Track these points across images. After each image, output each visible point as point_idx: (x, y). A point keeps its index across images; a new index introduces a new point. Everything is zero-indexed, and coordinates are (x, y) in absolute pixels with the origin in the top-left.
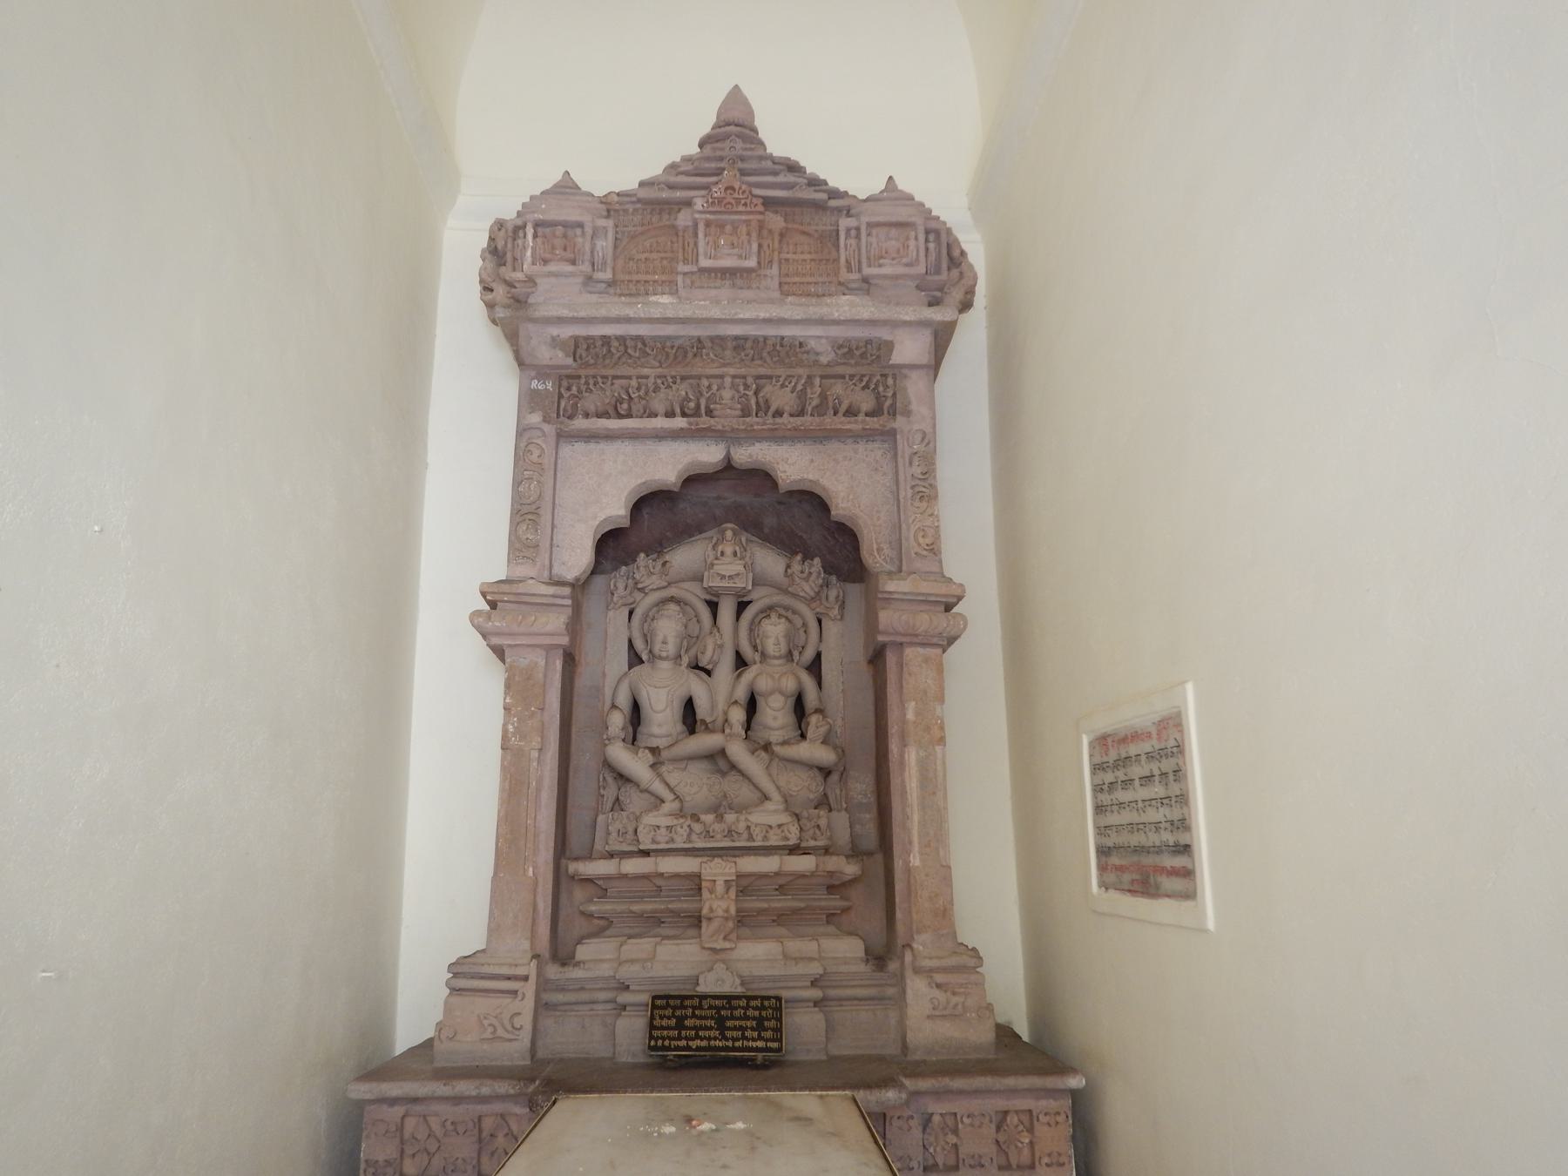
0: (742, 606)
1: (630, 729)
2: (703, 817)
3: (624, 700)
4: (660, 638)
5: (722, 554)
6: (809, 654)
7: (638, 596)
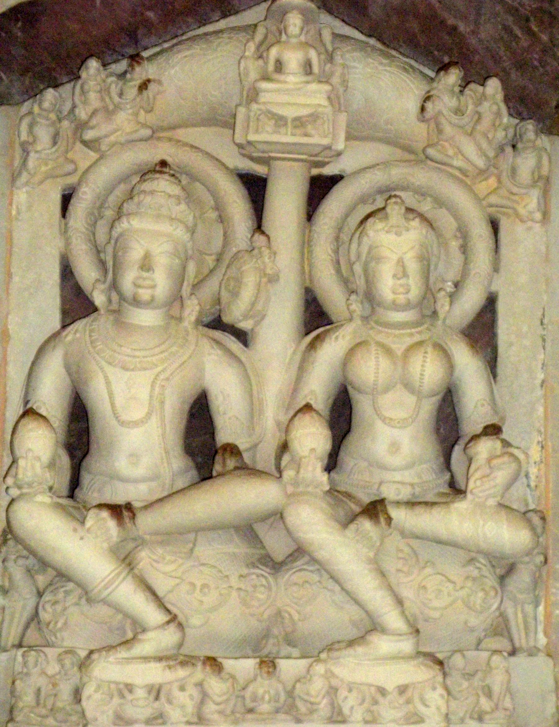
0: (320, 188)
1: (65, 461)
2: (229, 664)
3: (51, 396)
4: (136, 253)
5: (279, 66)
6: (470, 302)
7: (84, 157)
